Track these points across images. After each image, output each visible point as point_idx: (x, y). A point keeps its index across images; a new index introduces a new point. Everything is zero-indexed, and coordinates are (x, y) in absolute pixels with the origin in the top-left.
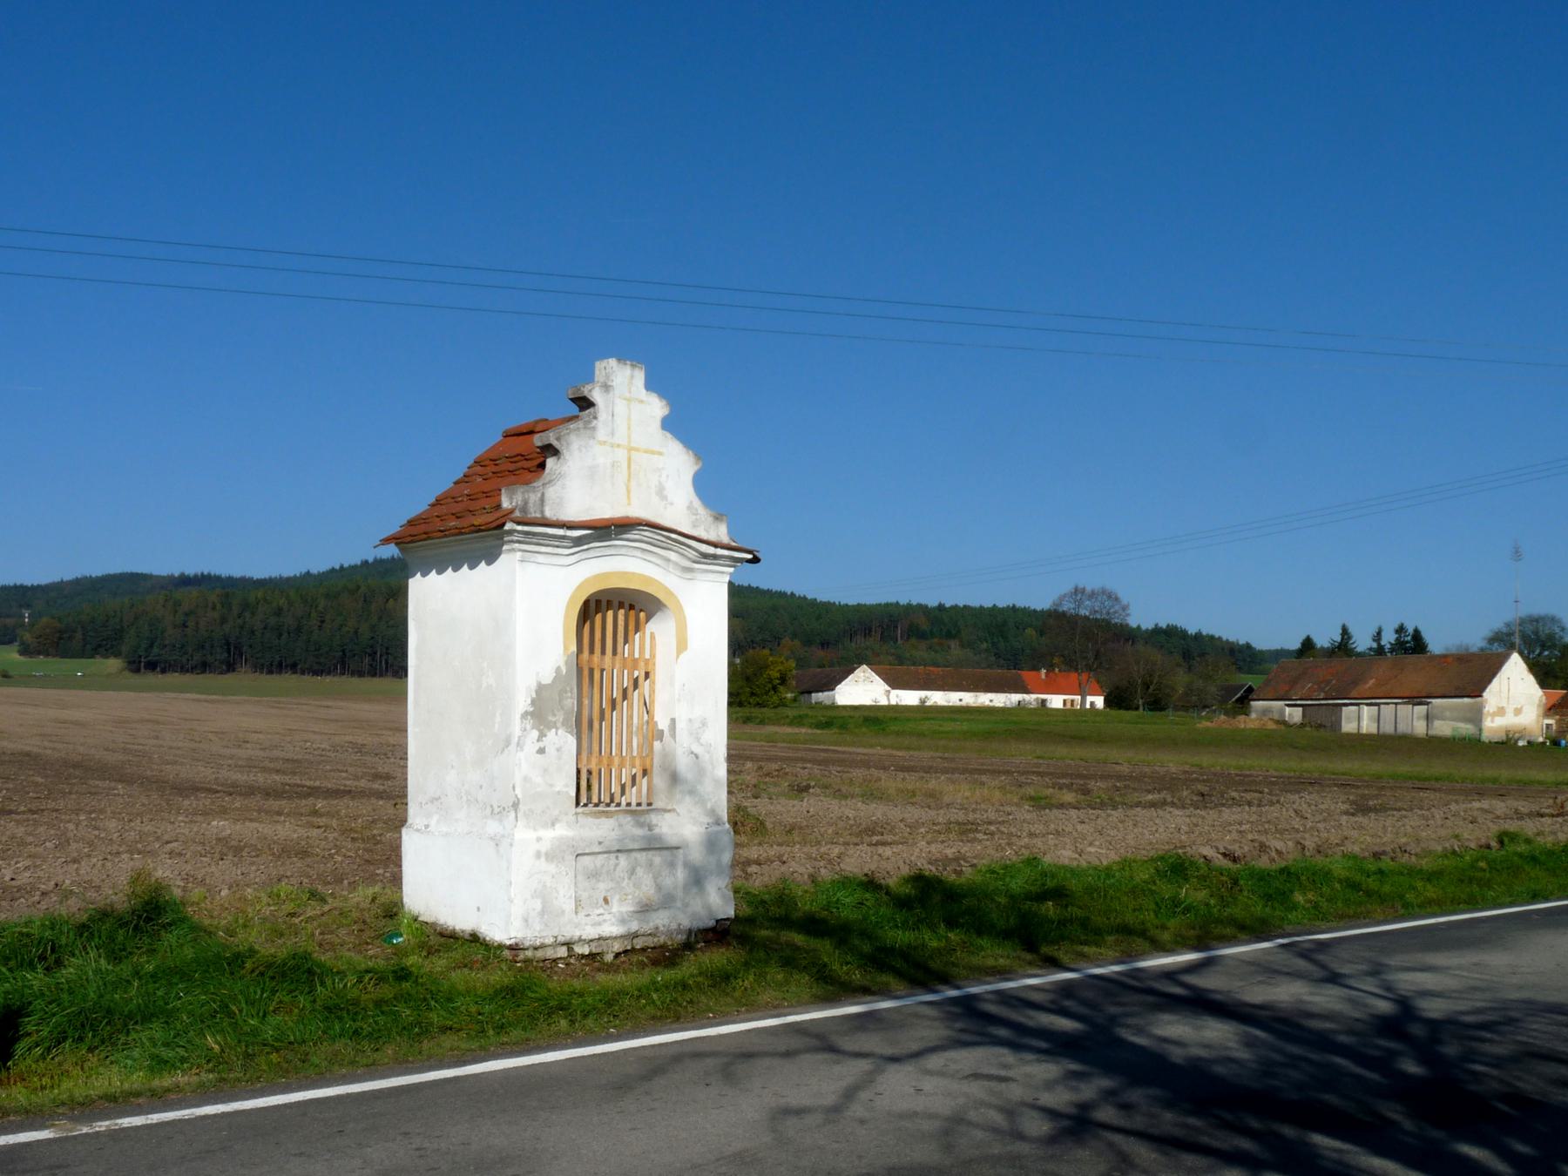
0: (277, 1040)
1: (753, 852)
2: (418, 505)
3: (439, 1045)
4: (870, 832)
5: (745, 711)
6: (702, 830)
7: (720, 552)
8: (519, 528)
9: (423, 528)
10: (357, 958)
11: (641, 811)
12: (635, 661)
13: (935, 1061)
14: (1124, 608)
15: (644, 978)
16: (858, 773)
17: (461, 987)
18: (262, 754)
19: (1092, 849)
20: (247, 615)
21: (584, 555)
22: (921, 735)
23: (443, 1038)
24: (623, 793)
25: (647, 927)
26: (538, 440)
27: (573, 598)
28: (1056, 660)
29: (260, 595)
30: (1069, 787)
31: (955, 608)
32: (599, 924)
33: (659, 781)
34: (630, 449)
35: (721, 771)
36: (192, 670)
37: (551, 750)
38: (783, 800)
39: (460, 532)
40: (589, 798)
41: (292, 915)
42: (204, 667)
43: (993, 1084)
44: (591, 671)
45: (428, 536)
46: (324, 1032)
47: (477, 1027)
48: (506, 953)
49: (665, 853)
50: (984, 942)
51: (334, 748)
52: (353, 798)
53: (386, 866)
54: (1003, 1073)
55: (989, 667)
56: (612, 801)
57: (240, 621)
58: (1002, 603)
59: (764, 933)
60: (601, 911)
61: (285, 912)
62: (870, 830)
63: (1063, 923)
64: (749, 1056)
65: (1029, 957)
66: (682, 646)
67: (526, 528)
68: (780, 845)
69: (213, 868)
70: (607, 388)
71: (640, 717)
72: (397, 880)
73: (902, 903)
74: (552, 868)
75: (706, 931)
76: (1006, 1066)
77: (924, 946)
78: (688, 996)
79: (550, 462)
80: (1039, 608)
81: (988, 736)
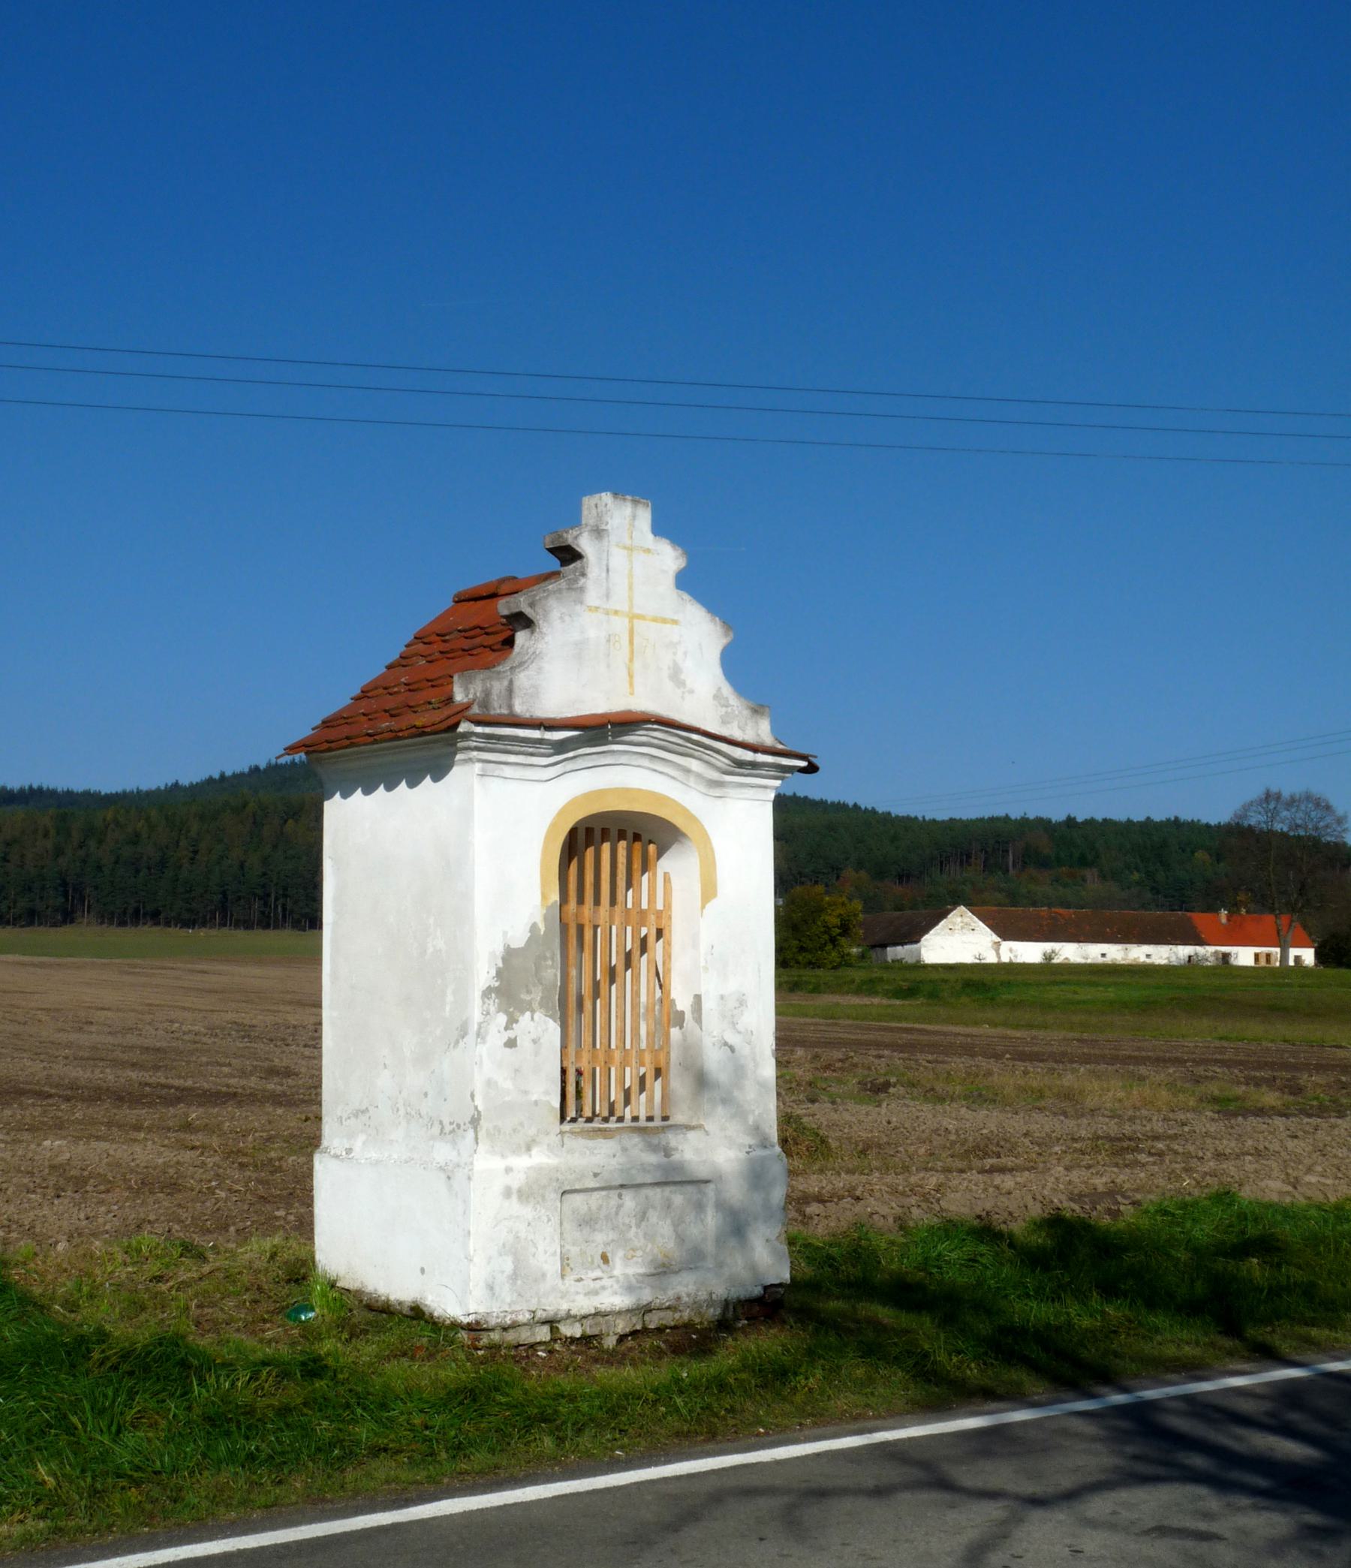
0: (138, 1468)
1: (813, 1184)
2: (338, 697)
3: (369, 1475)
4: (982, 1153)
5: (794, 973)
6: (742, 1155)
7: (761, 758)
8: (479, 729)
9: (346, 730)
10: (250, 1342)
11: (655, 1129)
12: (643, 914)
13: (1099, 1505)
14: (1340, 821)
15: (662, 1373)
16: (958, 1064)
17: (398, 1386)
18: (110, 1039)
19: (1312, 1179)
20: (92, 844)
21: (569, 766)
22: (1047, 1007)
23: (375, 1464)
24: (627, 1101)
25: (665, 1298)
26: (504, 607)
27: (553, 826)
28: (1241, 897)
29: (109, 816)
30: (1271, 1082)
31: (1090, 823)
32: (596, 1293)
33: (679, 1084)
34: (633, 617)
35: (768, 1070)
36: (14, 922)
37: (524, 1042)
38: (851, 1105)
39: (395, 736)
40: (579, 1110)
41: (159, 1279)
42: (31, 918)
43: (1189, 1544)
44: (580, 929)
45: (351, 741)
46: (204, 1456)
47: (424, 1448)
48: (463, 1335)
49: (690, 1189)
50: (1158, 1320)
51: (212, 1031)
52: (240, 1104)
53: (288, 1206)
54: (1203, 1526)
55: (1144, 907)
56: (612, 1113)
57: (81, 853)
58: (1160, 815)
59: (834, 1305)
60: (598, 1273)
61: (148, 1275)
62: (981, 1150)
63: (1276, 1291)
64: (821, 1494)
65: (1228, 1343)
66: (709, 891)
67: (488, 730)
68: (850, 1172)
69: (46, 1211)
70: (599, 533)
71: (650, 993)
72: (305, 1226)
73: (1033, 1259)
74: (527, 1212)
75: (750, 1302)
76: (1207, 1516)
77: (1070, 1324)
78: (728, 1401)
79: (521, 637)
80: (1213, 822)
81: (1146, 1007)
